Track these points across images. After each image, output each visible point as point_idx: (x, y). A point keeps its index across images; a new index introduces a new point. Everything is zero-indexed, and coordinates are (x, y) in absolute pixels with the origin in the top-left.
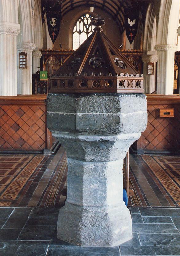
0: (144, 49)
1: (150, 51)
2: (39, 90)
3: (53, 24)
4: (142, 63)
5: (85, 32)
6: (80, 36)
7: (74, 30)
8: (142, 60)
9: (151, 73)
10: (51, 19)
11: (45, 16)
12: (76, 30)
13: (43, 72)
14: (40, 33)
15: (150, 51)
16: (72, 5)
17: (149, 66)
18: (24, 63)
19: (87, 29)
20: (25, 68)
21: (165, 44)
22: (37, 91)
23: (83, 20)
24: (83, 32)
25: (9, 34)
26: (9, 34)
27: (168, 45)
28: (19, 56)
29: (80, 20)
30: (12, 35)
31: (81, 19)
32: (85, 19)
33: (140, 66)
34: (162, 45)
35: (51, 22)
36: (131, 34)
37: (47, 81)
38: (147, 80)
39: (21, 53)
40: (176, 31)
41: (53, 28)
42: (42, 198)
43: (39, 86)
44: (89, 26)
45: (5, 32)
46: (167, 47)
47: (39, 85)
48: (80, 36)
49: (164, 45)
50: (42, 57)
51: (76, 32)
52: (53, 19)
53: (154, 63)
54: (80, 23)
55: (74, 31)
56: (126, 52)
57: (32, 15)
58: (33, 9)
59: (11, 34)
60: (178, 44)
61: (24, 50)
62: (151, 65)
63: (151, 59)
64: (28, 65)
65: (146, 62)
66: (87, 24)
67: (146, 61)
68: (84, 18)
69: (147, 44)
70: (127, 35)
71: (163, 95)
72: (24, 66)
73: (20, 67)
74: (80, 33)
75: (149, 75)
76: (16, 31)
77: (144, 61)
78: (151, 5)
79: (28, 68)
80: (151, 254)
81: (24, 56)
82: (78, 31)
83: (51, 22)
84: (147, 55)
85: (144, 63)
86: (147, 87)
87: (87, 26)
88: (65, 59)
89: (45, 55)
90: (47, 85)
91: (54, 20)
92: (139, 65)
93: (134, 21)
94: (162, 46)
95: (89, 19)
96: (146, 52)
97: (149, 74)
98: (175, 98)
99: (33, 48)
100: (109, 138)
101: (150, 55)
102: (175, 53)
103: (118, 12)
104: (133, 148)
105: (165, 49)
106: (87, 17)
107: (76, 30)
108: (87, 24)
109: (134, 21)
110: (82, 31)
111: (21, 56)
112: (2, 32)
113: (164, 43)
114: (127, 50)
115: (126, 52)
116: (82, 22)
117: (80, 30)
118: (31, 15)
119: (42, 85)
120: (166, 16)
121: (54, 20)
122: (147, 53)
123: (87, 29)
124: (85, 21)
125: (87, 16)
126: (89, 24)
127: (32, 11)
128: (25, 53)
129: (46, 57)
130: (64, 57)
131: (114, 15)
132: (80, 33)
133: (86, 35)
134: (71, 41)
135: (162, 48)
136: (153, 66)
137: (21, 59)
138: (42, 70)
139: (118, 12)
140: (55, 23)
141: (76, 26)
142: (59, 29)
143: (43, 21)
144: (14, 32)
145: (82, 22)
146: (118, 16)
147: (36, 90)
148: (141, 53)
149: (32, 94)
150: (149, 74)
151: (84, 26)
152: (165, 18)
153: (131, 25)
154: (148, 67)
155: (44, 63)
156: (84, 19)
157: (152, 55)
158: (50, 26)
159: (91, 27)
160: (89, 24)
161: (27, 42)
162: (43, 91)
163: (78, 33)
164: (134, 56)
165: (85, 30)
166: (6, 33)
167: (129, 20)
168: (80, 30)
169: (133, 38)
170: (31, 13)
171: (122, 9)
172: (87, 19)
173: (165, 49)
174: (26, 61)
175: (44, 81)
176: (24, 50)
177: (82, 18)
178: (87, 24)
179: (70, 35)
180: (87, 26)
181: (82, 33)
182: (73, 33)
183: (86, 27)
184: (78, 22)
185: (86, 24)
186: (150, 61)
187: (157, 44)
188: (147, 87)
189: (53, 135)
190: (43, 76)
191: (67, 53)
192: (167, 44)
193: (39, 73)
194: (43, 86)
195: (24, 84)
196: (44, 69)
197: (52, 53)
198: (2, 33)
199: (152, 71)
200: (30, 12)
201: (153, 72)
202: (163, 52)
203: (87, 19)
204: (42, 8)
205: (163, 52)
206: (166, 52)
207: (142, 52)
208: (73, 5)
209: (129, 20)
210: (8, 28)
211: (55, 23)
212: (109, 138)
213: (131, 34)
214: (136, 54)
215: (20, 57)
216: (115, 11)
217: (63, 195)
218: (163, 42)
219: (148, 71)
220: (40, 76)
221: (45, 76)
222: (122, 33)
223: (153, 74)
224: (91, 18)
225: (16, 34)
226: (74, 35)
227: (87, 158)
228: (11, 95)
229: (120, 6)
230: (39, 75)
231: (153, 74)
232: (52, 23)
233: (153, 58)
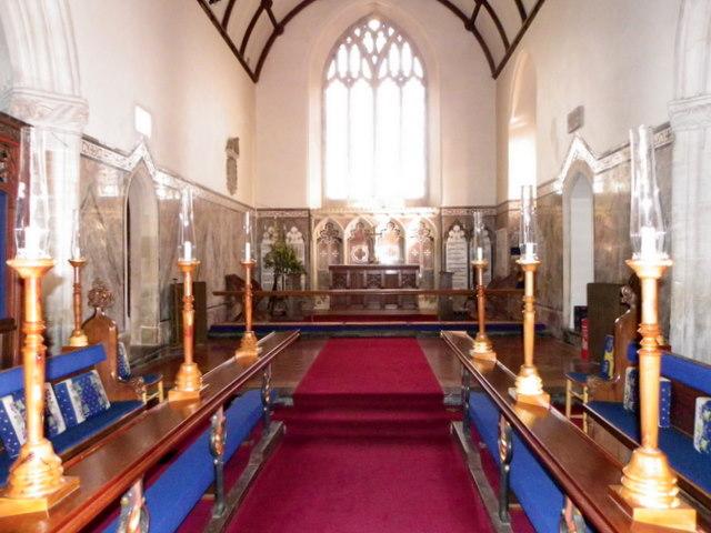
5: (418, 78)
6: (349, 95)
19: (375, 69)
23: (358, 41)
24: (413, 79)
32: (368, 35)
42: (53, 92)
48: (349, 95)
51: (388, 80)
74: (349, 81)
82: (343, 75)
84: (586, 308)
87: (375, 59)
95: (381, 34)
100: (239, 334)
104: (182, 304)
107: (389, 74)
108: (375, 52)
116: (355, 48)
123: (375, 69)
124: (368, 41)
132: (349, 81)
141: (336, 62)
145: (355, 48)
151: (365, 61)
163: (394, 83)
165: (368, 73)
172: (374, 36)
177: (357, 32)
178: (375, 52)
180: (375, 59)
181: (408, 83)
182: (325, 84)
183: (370, 61)
184: (343, 47)
189: (519, 505)
203: (374, 36)
212: (239, 334)
224: (386, 31)
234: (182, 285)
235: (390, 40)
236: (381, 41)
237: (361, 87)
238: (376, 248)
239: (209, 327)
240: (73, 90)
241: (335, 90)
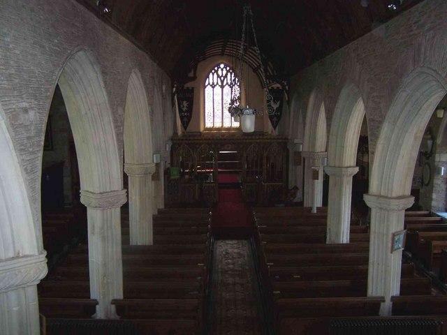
3: (184, 109)
12: (209, 84)
19: (222, 82)
23: (217, 72)
36: (275, 118)
54: (213, 74)
74: (213, 86)
80: (226, 148)
91: (185, 104)
98: (350, 255)
107: (209, 84)
108: (222, 76)
117: (213, 83)
121: (185, 104)
123: (222, 82)
124: (220, 72)
132: (213, 86)
142: (191, 114)
165: (220, 84)
168: (213, 83)
169: (277, 122)
172: (222, 70)
177: (216, 68)
180: (222, 78)
182: (205, 87)
203: (222, 70)
213: (275, 118)
217: (355, 177)
227: (440, 206)
234: (422, 210)
235: (228, 71)
236: (225, 72)
237: (218, 89)
238: (36, 266)
239: (118, 317)
240: (7, 296)
241: (208, 90)
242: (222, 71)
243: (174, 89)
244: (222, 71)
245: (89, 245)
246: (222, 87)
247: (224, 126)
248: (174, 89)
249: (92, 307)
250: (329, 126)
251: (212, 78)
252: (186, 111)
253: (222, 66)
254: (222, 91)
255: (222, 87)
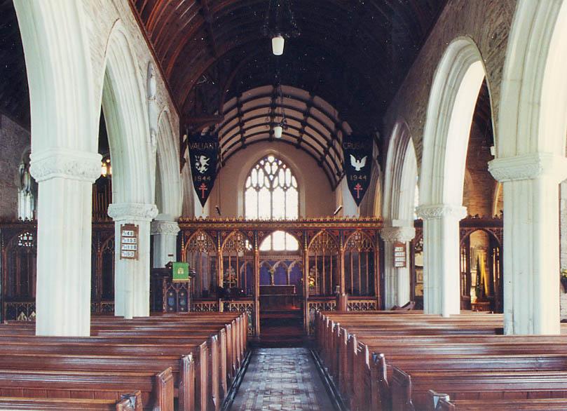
0: (385, 215)
1: (397, 219)
2: (171, 302)
3: (203, 169)
4: (382, 244)
7: (248, 185)
8: (382, 237)
9: (402, 264)
10: (199, 159)
11: (187, 154)
12: (252, 185)
13: (180, 264)
14: (175, 185)
15: (397, 219)
16: (243, 139)
17: (396, 250)
18: (131, 247)
19: (271, 182)
20: (133, 258)
21: (439, 204)
22: (168, 303)
23: (263, 167)
25: (72, 177)
26: (72, 177)
27: (445, 206)
28: (121, 233)
29: (258, 166)
30: (79, 181)
31: (260, 165)
32: (268, 164)
33: (378, 250)
34: (431, 204)
35: (198, 164)
36: (358, 186)
37: (187, 283)
38: (393, 278)
39: (126, 224)
40: (188, 273)
41: (202, 175)
43: (171, 294)
44: (274, 176)
45: (61, 172)
46: (444, 209)
47: (172, 290)
49: (435, 204)
50: (179, 233)
52: (202, 157)
53: (405, 244)
54: (258, 170)
55: (247, 186)
56: (348, 222)
57: (152, 145)
58: (153, 132)
59: (79, 178)
60: (558, 186)
61: (132, 218)
62: (401, 248)
63: (400, 236)
64: (141, 252)
65: (391, 242)
66: (271, 174)
67: (389, 239)
68: (265, 162)
69: (391, 209)
70: (349, 188)
71: (512, 335)
72: (132, 254)
73: (123, 255)
74: (258, 189)
75: (397, 267)
76: (91, 171)
77: (385, 240)
78: (399, 126)
79: (140, 257)
81: (131, 233)
82: (255, 186)
83: (198, 164)
85: (386, 243)
86: (393, 292)
87: (271, 177)
88: (226, 237)
89: (188, 228)
90: (189, 291)
92: (376, 247)
93: (364, 160)
94: (432, 207)
95: (275, 164)
96: (390, 222)
97: (396, 265)
99: (151, 215)
101: (397, 228)
102: (460, 222)
103: (327, 151)
105: (440, 215)
106: (271, 161)
107: (252, 185)
108: (271, 174)
109: (364, 160)
110: (261, 186)
111: (126, 232)
112: (53, 172)
113: (436, 200)
114: (351, 218)
115: (348, 222)
116: (261, 170)
117: (258, 185)
118: (149, 144)
119: (177, 291)
120: (439, 142)
121: (203, 161)
122: (391, 223)
123: (271, 182)
124: (267, 168)
125: (271, 159)
126: (274, 173)
127: (151, 137)
128: (134, 225)
129: (187, 234)
130: (223, 234)
131: (319, 156)
132: (258, 189)
133: (269, 193)
134: (242, 204)
135: (432, 213)
136: (405, 250)
137: (126, 238)
138: (179, 259)
139: (327, 151)
140: (205, 166)
142: (213, 178)
143: (183, 161)
144: (83, 173)
145: (261, 170)
146: (327, 157)
147: (165, 302)
148: (379, 224)
149: (148, 315)
150: (396, 265)
151: (266, 178)
152: (436, 148)
153: (358, 169)
154: (393, 252)
155: (185, 245)
156: (265, 165)
157: (401, 227)
158: (195, 172)
159: (272, 238)
160: (274, 173)
161: (139, 201)
162: (180, 305)
164: (364, 229)
165: (268, 185)
166: (65, 176)
167: (353, 159)
168: (258, 185)
170: (149, 141)
171: (340, 136)
172: (271, 164)
173: (440, 215)
174: (137, 244)
175: (181, 283)
176: (132, 218)
177: (262, 162)
179: (240, 194)
180: (271, 177)
181: (261, 190)
182: (245, 189)
183: (269, 179)
184: (254, 170)
185: (269, 173)
186: (399, 240)
187: (422, 203)
188: (393, 292)
190: (179, 273)
191: (230, 226)
192: (444, 201)
193: (172, 266)
194: (179, 293)
195: (132, 294)
196: (184, 257)
197: (200, 225)
198: (52, 175)
199: (402, 259)
200: (146, 138)
201: (405, 263)
202: (435, 220)
203: (271, 164)
204: (181, 138)
205: (435, 220)
206: (441, 219)
207: (381, 222)
208: (245, 140)
209: (353, 159)
210: (69, 163)
211: (205, 166)
213: (358, 186)
214: (369, 225)
215: (123, 235)
216: (321, 150)
218: (433, 200)
219: (394, 260)
220: (174, 273)
221: (182, 273)
222: (334, 186)
223: (405, 266)
224: (277, 162)
225: (92, 177)
226: (246, 193)
228: (74, 334)
229: (326, 146)
230: (171, 271)
231: (405, 266)
232: (200, 165)
233: (404, 235)
235: (280, 167)
237: (265, 192)
241: (250, 193)
242: (271, 164)
243: (185, 137)
244: (271, 164)
245: (477, 98)
246: (271, 189)
247: (293, 215)
248: (185, 137)
249: (367, 158)
250: (419, 190)
251: (257, 177)
252: (206, 173)
253: (271, 159)
254: (272, 194)
255: (271, 189)
